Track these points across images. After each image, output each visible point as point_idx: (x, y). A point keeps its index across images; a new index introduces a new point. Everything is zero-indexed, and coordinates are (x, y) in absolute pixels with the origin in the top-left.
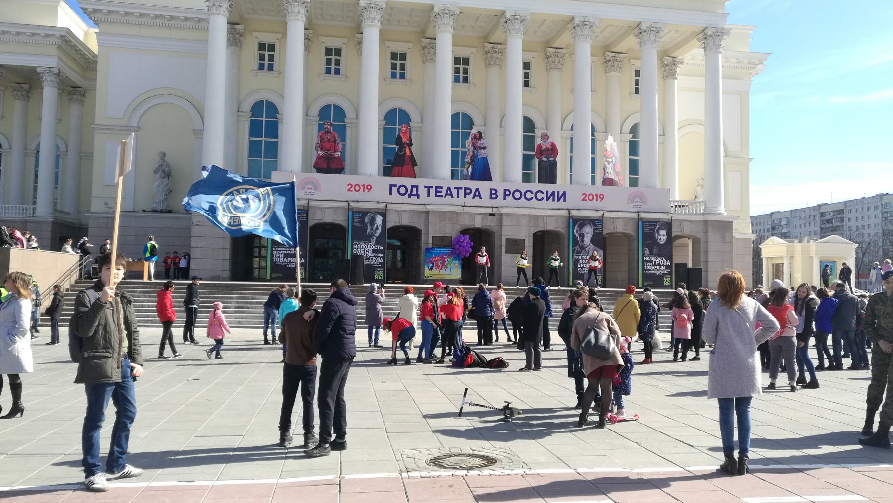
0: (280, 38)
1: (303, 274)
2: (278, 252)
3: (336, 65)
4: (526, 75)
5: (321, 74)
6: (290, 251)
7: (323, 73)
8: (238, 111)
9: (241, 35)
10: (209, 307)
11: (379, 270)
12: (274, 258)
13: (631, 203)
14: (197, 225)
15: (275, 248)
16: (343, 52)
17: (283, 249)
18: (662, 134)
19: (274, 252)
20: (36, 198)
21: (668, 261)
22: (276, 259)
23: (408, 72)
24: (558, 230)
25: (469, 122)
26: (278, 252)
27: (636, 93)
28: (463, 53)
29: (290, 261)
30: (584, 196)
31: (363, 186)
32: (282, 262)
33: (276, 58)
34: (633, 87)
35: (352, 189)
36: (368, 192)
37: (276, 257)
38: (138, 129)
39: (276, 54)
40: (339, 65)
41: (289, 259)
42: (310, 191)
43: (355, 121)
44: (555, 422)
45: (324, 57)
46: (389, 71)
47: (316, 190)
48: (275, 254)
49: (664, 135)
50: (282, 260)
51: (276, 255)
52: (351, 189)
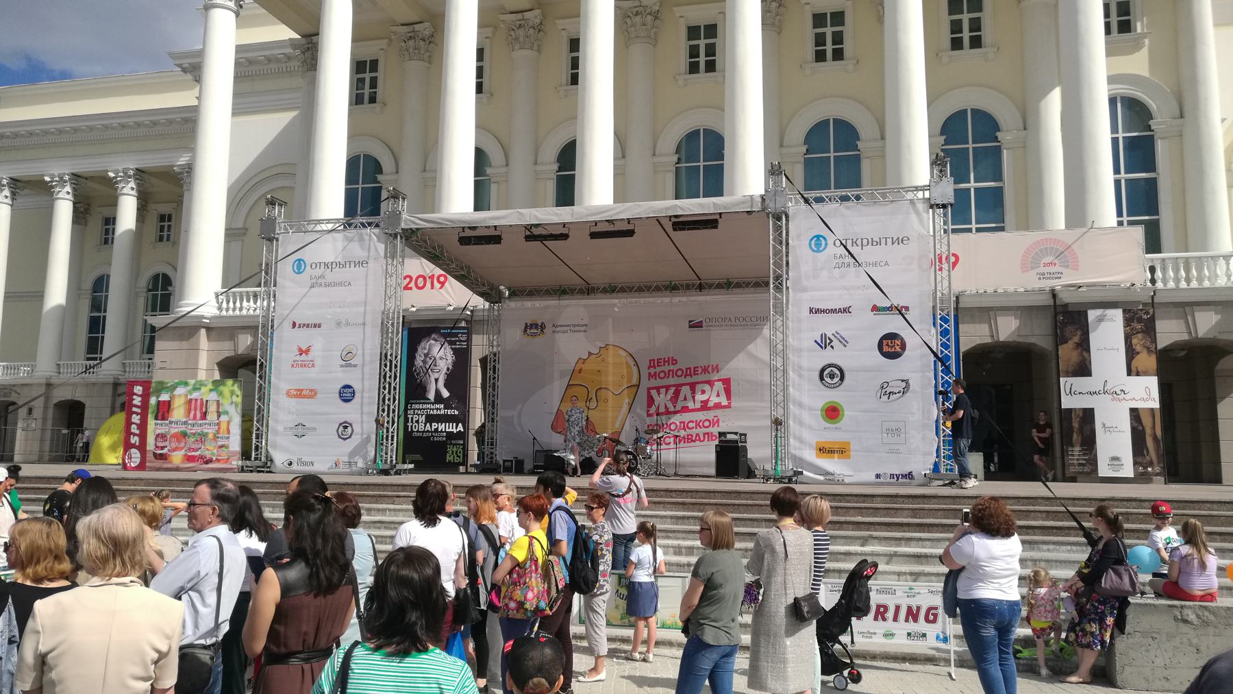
0: (384, 47)
1: (461, 455)
2: (416, 411)
3: (971, 30)
4: (480, 72)
5: (561, 85)
6: (437, 409)
7: (564, 82)
8: (536, 163)
9: (656, 18)
10: (826, 554)
11: (456, 444)
12: (410, 424)
13: (1032, 268)
14: (161, 368)
15: (412, 404)
16: (848, 18)
17: (425, 406)
18: (1178, 114)
19: (409, 412)
20: (836, 309)
21: (460, 425)
22: (412, 426)
23: (987, 33)
24: (1033, 340)
25: (375, 167)
26: (416, 411)
27: (691, 72)
28: (371, 51)
29: (436, 430)
30: (408, 279)
31: (432, 277)
32: (423, 432)
33: (380, 83)
34: (486, 64)
35: (412, 285)
36: (441, 288)
37: (412, 422)
38: (243, 231)
39: (718, 41)
40: (979, 29)
41: (435, 425)
42: (1052, 269)
43: (504, 170)
44: (993, 183)
45: (809, 33)
46: (946, 36)
47: (1067, 267)
48: (410, 416)
49: (1025, 129)
50: (421, 427)
51: (412, 418)
52: (410, 286)
